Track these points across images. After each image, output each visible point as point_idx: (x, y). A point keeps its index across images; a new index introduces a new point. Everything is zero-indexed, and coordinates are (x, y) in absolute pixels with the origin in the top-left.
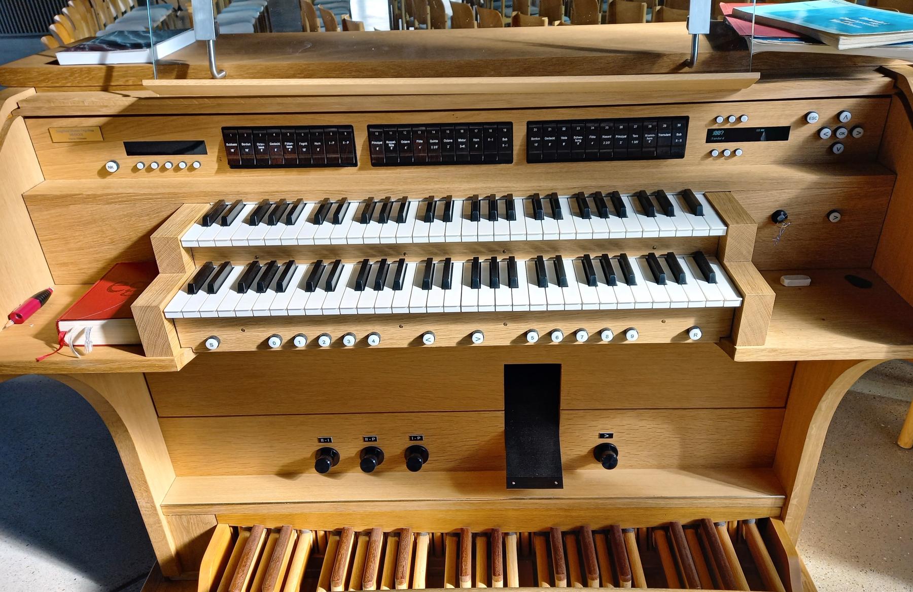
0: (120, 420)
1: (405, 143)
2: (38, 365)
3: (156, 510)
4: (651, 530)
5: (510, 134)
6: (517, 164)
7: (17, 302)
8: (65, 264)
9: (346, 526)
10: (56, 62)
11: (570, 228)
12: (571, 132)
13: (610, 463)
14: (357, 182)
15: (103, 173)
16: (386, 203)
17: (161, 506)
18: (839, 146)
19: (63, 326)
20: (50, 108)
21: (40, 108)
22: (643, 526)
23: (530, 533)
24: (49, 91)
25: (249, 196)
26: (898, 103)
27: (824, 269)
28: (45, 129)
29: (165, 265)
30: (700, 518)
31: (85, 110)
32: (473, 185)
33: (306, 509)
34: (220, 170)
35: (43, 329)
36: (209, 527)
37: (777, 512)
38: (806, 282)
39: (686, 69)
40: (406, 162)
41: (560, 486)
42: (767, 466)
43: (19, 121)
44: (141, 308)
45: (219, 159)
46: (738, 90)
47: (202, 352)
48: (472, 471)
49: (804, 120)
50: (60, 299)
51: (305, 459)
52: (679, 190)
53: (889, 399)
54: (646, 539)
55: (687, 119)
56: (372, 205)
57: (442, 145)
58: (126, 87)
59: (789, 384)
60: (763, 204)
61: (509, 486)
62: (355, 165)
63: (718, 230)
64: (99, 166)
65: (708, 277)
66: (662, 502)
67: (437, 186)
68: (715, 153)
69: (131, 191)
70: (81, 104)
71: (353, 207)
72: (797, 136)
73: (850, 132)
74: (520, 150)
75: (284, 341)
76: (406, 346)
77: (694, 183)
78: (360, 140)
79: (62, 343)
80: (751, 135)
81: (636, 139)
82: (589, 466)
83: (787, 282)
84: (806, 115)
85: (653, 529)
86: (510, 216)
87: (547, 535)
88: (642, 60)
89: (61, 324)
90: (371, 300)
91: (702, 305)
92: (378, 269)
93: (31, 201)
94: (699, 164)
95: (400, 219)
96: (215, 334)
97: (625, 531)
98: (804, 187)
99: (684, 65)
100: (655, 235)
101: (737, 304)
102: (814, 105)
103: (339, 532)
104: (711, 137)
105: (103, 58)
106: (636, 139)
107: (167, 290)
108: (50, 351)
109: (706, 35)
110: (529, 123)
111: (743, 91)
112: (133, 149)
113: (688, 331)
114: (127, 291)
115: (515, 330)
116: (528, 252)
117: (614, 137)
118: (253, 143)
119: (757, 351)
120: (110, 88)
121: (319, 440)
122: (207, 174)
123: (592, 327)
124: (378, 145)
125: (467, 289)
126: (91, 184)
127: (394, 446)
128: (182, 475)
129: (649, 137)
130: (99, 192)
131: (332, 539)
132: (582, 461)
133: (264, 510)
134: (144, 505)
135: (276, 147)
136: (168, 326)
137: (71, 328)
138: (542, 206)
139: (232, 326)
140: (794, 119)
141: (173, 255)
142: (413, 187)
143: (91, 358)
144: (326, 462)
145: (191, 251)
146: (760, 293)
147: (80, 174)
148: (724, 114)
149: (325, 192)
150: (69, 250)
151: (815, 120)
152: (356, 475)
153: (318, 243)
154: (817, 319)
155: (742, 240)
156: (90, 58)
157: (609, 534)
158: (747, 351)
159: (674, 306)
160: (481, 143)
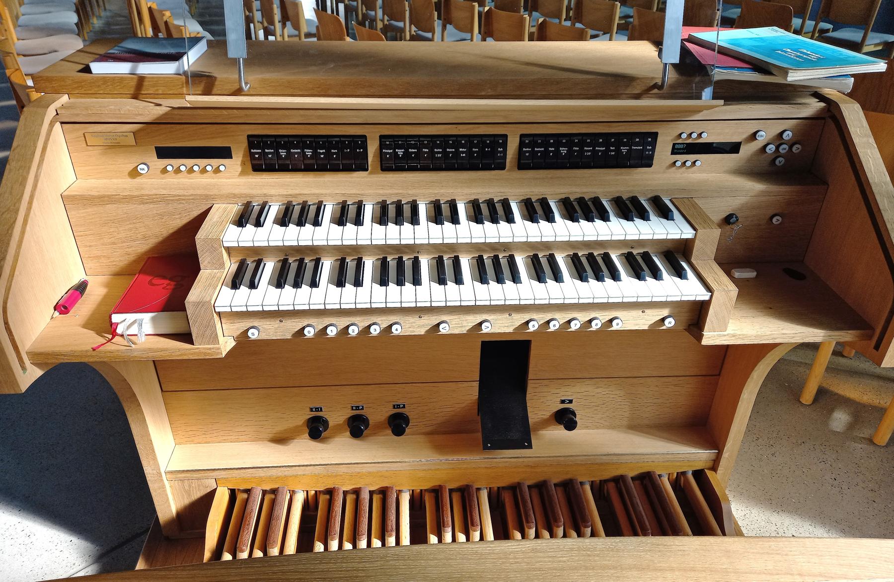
0: (134, 395)
1: (409, 152)
2: (94, 353)
4: (603, 482)
5: (504, 145)
6: (509, 170)
7: (59, 292)
8: (98, 257)
10: (87, 70)
12: (558, 144)
13: (571, 425)
14: (370, 186)
16: (304, 207)
18: (781, 159)
19: (116, 318)
20: (89, 115)
21: (77, 115)
22: (597, 479)
23: (498, 488)
24: (82, 97)
26: (832, 125)
27: (773, 265)
28: (81, 133)
31: (121, 118)
32: (474, 191)
33: (300, 471)
34: (243, 173)
35: (89, 319)
36: (209, 490)
37: (710, 464)
38: (752, 274)
39: (656, 91)
41: (530, 446)
42: (703, 424)
43: (58, 125)
45: (243, 163)
47: (243, 340)
48: (449, 434)
49: (753, 136)
50: (96, 292)
51: (297, 427)
52: (650, 196)
53: (790, 361)
54: (599, 489)
55: (656, 134)
56: (291, 208)
57: (444, 153)
58: (156, 95)
59: (730, 361)
60: (717, 209)
61: (485, 448)
62: (367, 170)
63: (687, 233)
64: (131, 167)
65: (679, 273)
66: (615, 458)
67: (442, 191)
68: (678, 164)
69: (164, 192)
70: (117, 112)
72: (747, 150)
73: (791, 147)
78: (372, 149)
79: (114, 334)
81: (612, 151)
83: (737, 274)
84: (755, 133)
86: (414, 220)
87: (514, 489)
88: (615, 83)
89: (113, 316)
92: (296, 268)
93: (69, 200)
94: (664, 172)
95: (316, 223)
96: (256, 324)
97: (582, 483)
99: (654, 89)
101: (707, 298)
102: (764, 124)
103: (330, 492)
104: (675, 151)
105: (134, 68)
106: (612, 151)
109: (674, 65)
110: (522, 136)
111: (705, 112)
112: (163, 153)
113: (663, 320)
114: (167, 285)
115: (519, 319)
117: (594, 148)
118: (273, 151)
119: (720, 336)
120: (141, 96)
121: (311, 410)
122: (230, 180)
123: (583, 317)
124: (388, 153)
125: (376, 287)
126: (122, 184)
127: (378, 414)
128: (180, 444)
129: (624, 150)
130: (136, 193)
131: (323, 499)
132: (544, 424)
133: (261, 473)
135: (296, 153)
138: (536, 211)
139: (274, 317)
140: (745, 136)
142: (421, 191)
144: (317, 429)
145: (229, 250)
146: (725, 290)
147: (110, 176)
148: (688, 130)
149: (343, 194)
150: (103, 244)
151: (763, 137)
152: (344, 440)
154: (766, 308)
155: (708, 241)
156: (123, 68)
157: (569, 487)
158: (711, 337)
160: (475, 152)
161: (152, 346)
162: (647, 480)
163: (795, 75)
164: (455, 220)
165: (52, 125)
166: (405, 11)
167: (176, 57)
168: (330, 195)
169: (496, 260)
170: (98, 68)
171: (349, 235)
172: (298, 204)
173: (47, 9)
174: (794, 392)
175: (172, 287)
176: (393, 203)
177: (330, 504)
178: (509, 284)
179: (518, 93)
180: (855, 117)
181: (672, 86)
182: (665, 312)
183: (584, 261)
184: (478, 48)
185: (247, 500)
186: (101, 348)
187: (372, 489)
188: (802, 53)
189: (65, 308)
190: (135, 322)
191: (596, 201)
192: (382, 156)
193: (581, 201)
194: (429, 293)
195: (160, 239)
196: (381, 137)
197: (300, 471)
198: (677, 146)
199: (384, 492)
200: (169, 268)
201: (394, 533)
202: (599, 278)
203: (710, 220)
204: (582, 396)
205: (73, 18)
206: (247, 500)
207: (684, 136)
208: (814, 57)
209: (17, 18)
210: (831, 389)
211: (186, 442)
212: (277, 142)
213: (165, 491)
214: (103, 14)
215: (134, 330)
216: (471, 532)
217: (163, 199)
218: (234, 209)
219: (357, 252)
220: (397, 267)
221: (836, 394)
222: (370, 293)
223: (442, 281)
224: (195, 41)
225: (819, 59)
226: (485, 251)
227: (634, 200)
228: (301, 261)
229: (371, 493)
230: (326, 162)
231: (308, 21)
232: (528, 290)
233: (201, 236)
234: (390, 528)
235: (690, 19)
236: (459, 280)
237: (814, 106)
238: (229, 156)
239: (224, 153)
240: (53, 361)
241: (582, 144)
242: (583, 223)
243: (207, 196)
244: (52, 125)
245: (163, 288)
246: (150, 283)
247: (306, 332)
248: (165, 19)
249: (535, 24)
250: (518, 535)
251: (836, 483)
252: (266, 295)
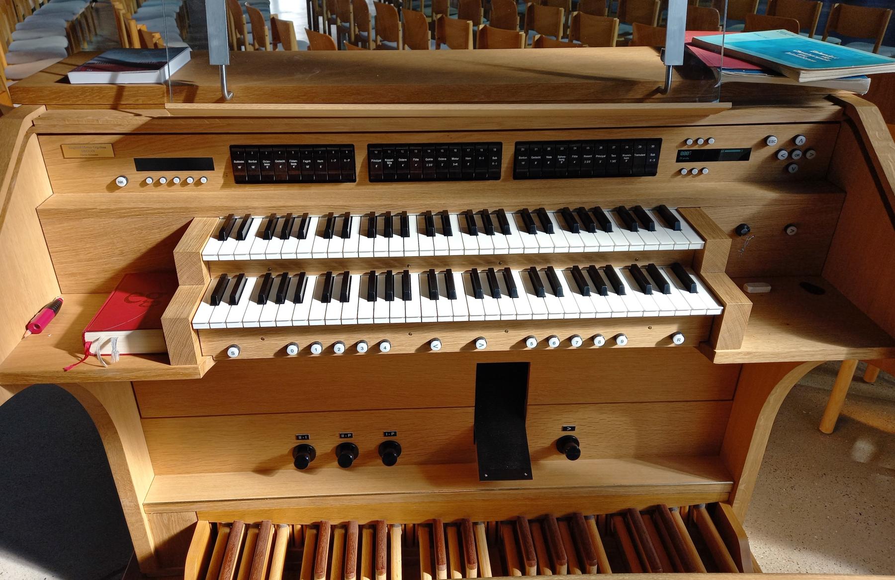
1: (401, 161)
2: (66, 374)
3: (139, 508)
4: (610, 517)
5: (499, 153)
6: (505, 180)
7: (32, 311)
9: (323, 520)
10: (66, 80)
11: (459, 243)
12: (555, 152)
14: (358, 198)
15: (113, 186)
16: (289, 219)
17: (144, 505)
18: (794, 166)
19: (89, 337)
21: (54, 126)
22: (603, 513)
23: (497, 522)
24: (59, 108)
25: (257, 211)
28: (58, 145)
29: (185, 277)
30: (656, 504)
33: (284, 504)
34: (225, 185)
35: (62, 338)
36: (189, 524)
37: (725, 497)
38: (768, 289)
39: (659, 95)
40: (402, 179)
41: (530, 477)
42: (716, 454)
43: (34, 137)
44: (171, 320)
45: (225, 175)
46: (707, 116)
47: (222, 357)
48: (442, 464)
49: (764, 142)
50: (71, 310)
51: (282, 456)
52: (654, 206)
54: (606, 524)
56: (275, 221)
57: (436, 163)
58: (136, 106)
59: (745, 383)
60: (728, 218)
61: (482, 478)
62: (354, 181)
63: (696, 244)
64: (109, 180)
65: (689, 287)
68: (684, 172)
69: (143, 205)
70: (95, 123)
71: (257, 223)
73: (804, 153)
74: (507, 168)
75: (325, 347)
76: (413, 352)
77: (668, 199)
78: (360, 159)
79: (87, 353)
80: (713, 155)
81: (614, 158)
82: (551, 457)
83: (750, 289)
85: (612, 515)
86: (404, 233)
87: (514, 523)
88: (617, 87)
90: (384, 310)
91: (687, 313)
92: (279, 282)
93: (44, 214)
95: (301, 236)
97: (586, 518)
98: (765, 203)
99: (656, 92)
100: (641, 249)
101: (718, 312)
102: (775, 129)
105: (114, 78)
106: (614, 158)
107: (191, 301)
108: (75, 361)
109: (676, 68)
110: (517, 144)
111: (711, 116)
112: (143, 165)
113: (671, 337)
114: (145, 302)
115: (516, 336)
116: (362, 268)
117: (594, 156)
118: (258, 160)
120: (120, 106)
121: (297, 438)
122: (211, 192)
124: (376, 163)
125: (364, 302)
126: (100, 198)
127: (367, 442)
129: (626, 157)
130: (113, 207)
131: (309, 534)
133: (244, 506)
134: (128, 504)
135: (281, 164)
136: (194, 335)
137: (96, 339)
138: (533, 222)
139: (253, 335)
141: (194, 268)
143: (118, 367)
144: (303, 458)
145: (208, 264)
146: (739, 303)
147: (88, 190)
149: (329, 207)
151: (775, 142)
152: (332, 470)
153: (269, 257)
155: (717, 254)
156: (101, 78)
157: (572, 521)
158: (724, 355)
159: (614, 315)
161: (127, 366)
162: (657, 514)
163: (808, 75)
164: (447, 232)
165: (27, 136)
166: (398, 30)
167: (158, 66)
168: (317, 207)
169: (490, 274)
170: (77, 78)
171: (336, 248)
172: (282, 217)
173: (36, 35)
174: (813, 419)
175: (149, 304)
176: (381, 215)
177: (317, 539)
178: (505, 298)
180: (872, 119)
181: (677, 90)
182: (673, 329)
183: (585, 274)
184: (471, 56)
185: (229, 534)
186: (74, 369)
187: (363, 523)
188: (813, 54)
189: (37, 326)
190: (108, 341)
191: (597, 212)
192: (369, 165)
193: (580, 211)
194: (418, 308)
195: (138, 255)
196: (369, 146)
197: (284, 504)
198: (682, 154)
199: (374, 527)
200: (146, 285)
201: (385, 571)
202: (602, 292)
203: (720, 230)
204: (585, 423)
205: (63, 43)
206: (229, 534)
207: (690, 142)
208: (827, 57)
209: (8, 43)
210: (853, 416)
211: (168, 473)
212: (261, 152)
213: (143, 525)
214: (94, 39)
215: (108, 350)
216: (468, 570)
217: (141, 213)
218: (217, 222)
219: (344, 266)
220: (385, 280)
221: (859, 423)
222: (357, 309)
223: (433, 296)
224: (176, 52)
225: (832, 60)
226: (479, 264)
227: (638, 210)
228: (284, 276)
229: (361, 528)
230: (312, 173)
231: (300, 43)
232: (525, 305)
233: (179, 250)
234: (380, 565)
235: (693, 23)
236: (451, 295)
237: (828, 110)
238: (212, 168)
239: (206, 165)
240: (23, 382)
241: (581, 151)
242: (583, 233)
243: (187, 208)
244: (27, 136)
245: (139, 305)
246: (127, 300)
247: (289, 351)
248: (154, 40)
249: (531, 42)
250: (518, 573)
251: (860, 517)
252: (247, 312)
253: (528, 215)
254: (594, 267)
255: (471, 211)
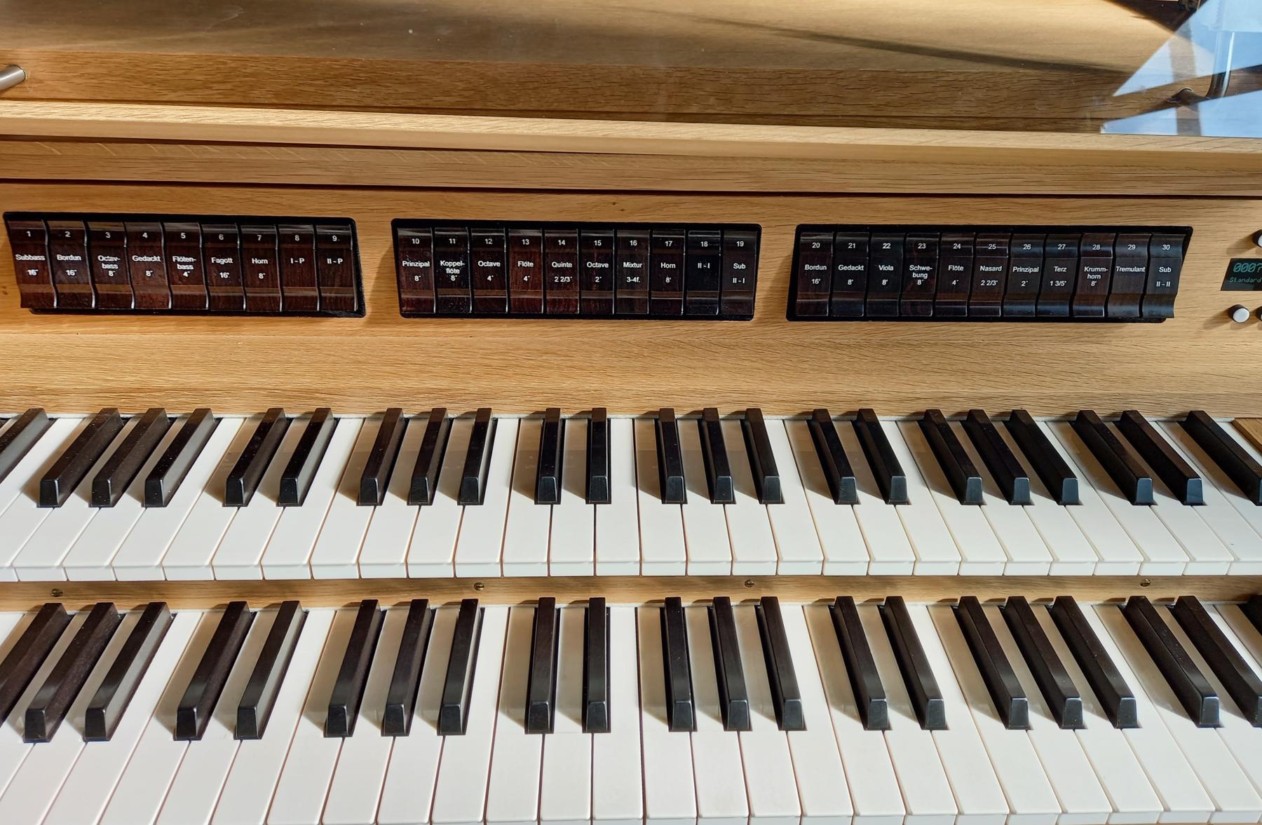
1: (477, 265)
5: (751, 254)
6: (761, 322)
14: (360, 365)
25: (62, 400)
52: (1173, 411)
55: (1187, 232)
62: (360, 313)
71: (347, 435)
78: (373, 257)
81: (1060, 276)
106: (1060, 276)
110: (801, 230)
138: (847, 458)
149: (271, 393)
179: (794, 110)
198: (1240, 268)
212: (471, 238)
253: (828, 427)
254: (974, 599)
255: (669, 412)
